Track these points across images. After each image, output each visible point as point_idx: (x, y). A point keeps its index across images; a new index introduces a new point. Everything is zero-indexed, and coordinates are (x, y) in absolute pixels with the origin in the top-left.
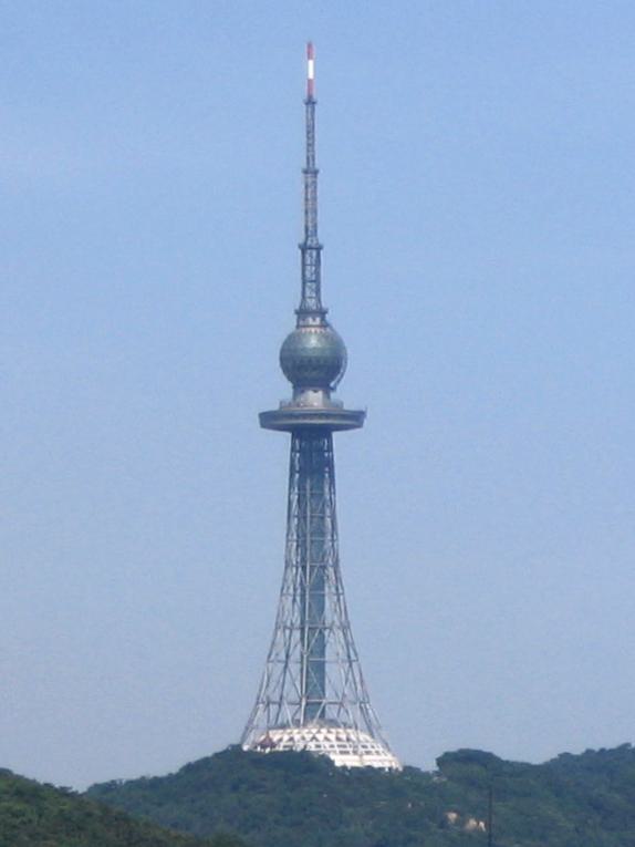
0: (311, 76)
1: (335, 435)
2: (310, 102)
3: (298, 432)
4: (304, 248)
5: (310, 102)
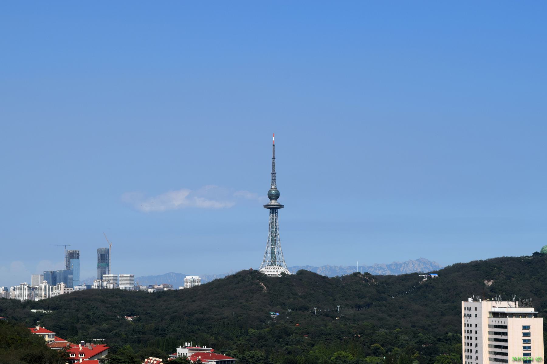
0: (274, 140)
1: (278, 209)
2: (274, 145)
3: (270, 208)
4: (273, 173)
5: (274, 145)
